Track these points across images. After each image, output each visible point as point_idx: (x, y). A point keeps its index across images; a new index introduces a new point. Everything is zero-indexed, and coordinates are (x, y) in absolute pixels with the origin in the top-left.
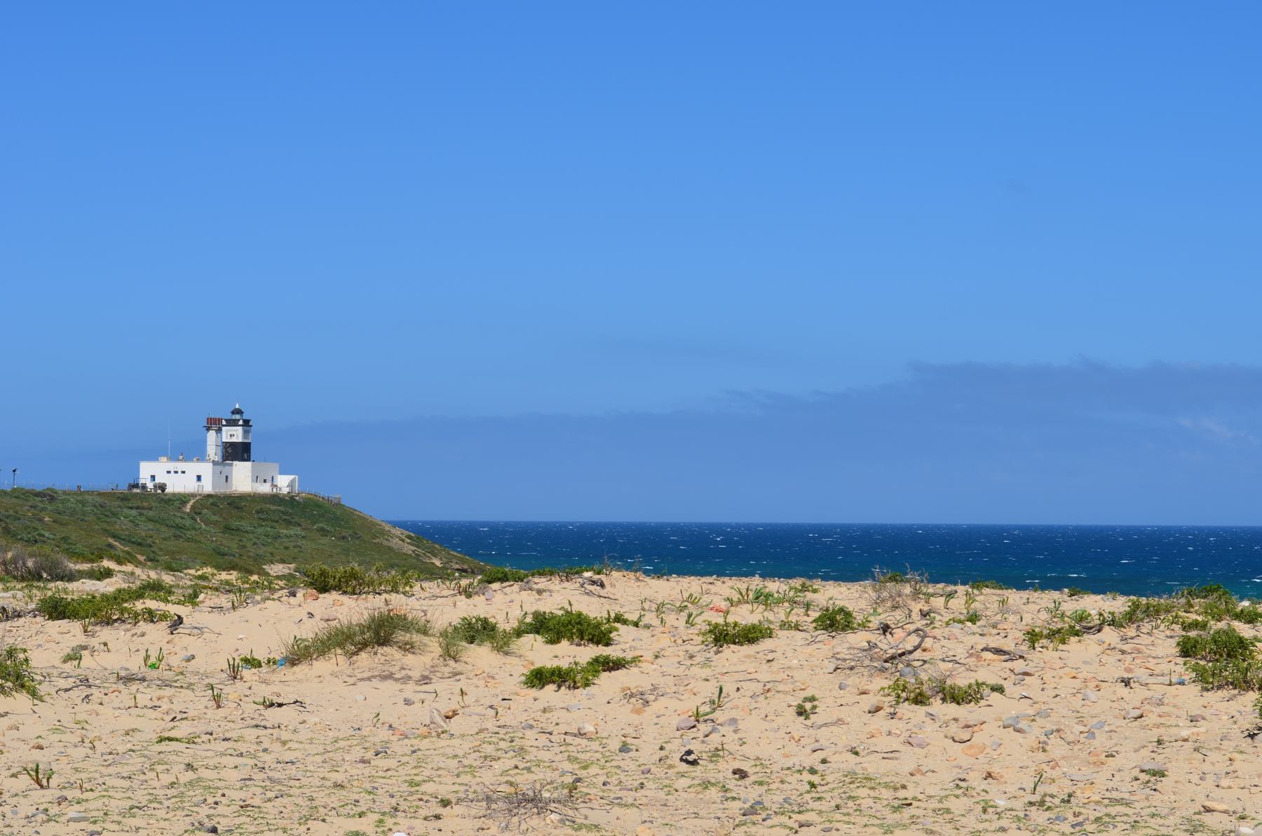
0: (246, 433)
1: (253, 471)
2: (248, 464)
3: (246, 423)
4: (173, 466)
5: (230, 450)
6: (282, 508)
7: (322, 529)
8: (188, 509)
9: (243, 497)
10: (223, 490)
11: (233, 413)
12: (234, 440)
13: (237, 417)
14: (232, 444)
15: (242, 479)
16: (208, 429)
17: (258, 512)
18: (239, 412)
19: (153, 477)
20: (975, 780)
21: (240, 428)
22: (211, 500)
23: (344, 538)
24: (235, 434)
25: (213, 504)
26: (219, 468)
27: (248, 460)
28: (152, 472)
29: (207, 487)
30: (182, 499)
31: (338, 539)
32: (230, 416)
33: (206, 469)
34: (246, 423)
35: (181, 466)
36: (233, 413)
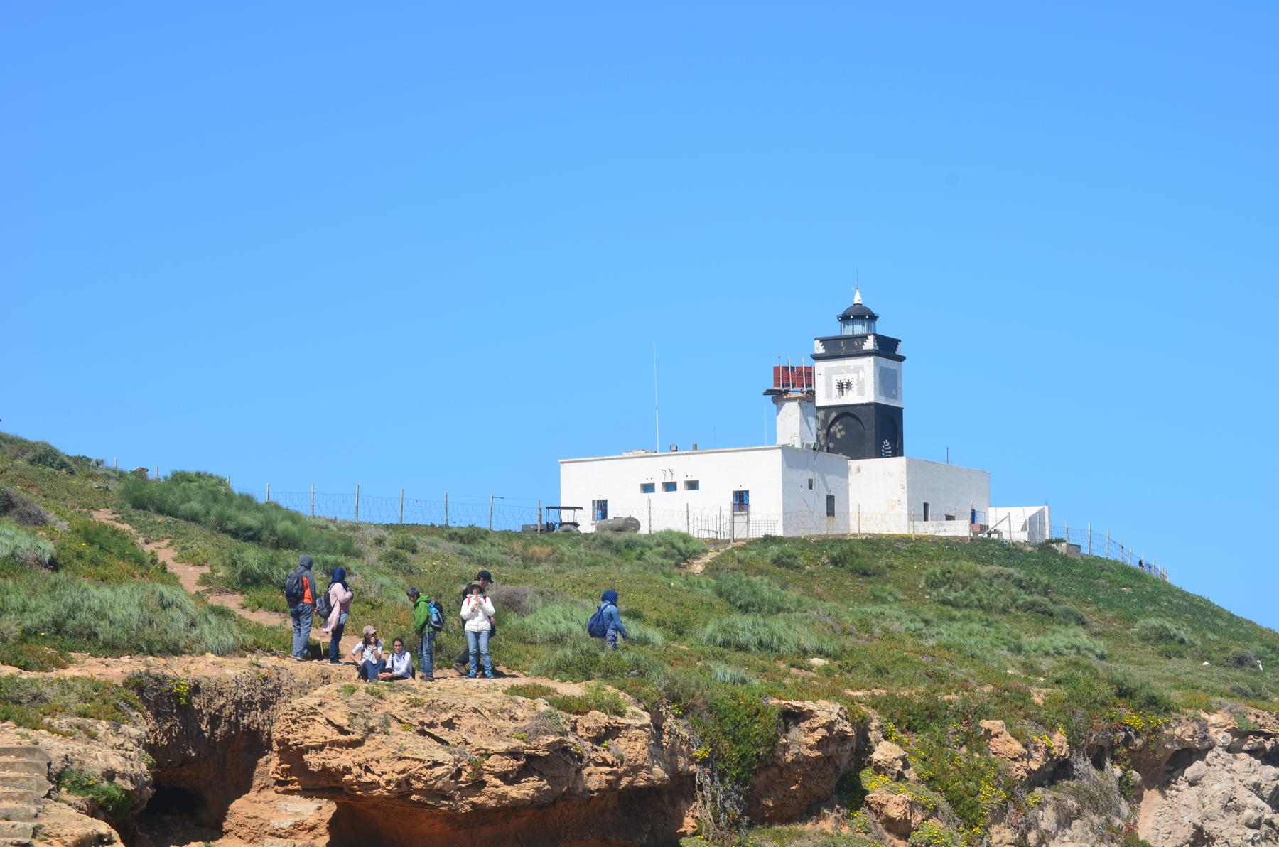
0: (887, 381)
1: (912, 486)
2: (892, 468)
3: (887, 348)
4: (655, 468)
5: (838, 431)
6: (1017, 573)
7: (1162, 636)
8: (697, 567)
9: (876, 543)
10: (816, 527)
11: (845, 319)
12: (851, 398)
13: (859, 329)
14: (845, 413)
15: (877, 497)
16: (778, 396)
17: (933, 584)
18: (863, 315)
19: (602, 507)
20: (1031, 746)
21: (868, 363)
22: (774, 550)
23: (1241, 661)
24: (856, 382)
25: (777, 562)
26: (803, 476)
27: (897, 451)
28: (597, 486)
29: (768, 517)
30: (678, 549)
31: (1226, 664)
32: (836, 329)
33: (762, 473)
34: (887, 348)
35: (683, 467)
36: (845, 319)
